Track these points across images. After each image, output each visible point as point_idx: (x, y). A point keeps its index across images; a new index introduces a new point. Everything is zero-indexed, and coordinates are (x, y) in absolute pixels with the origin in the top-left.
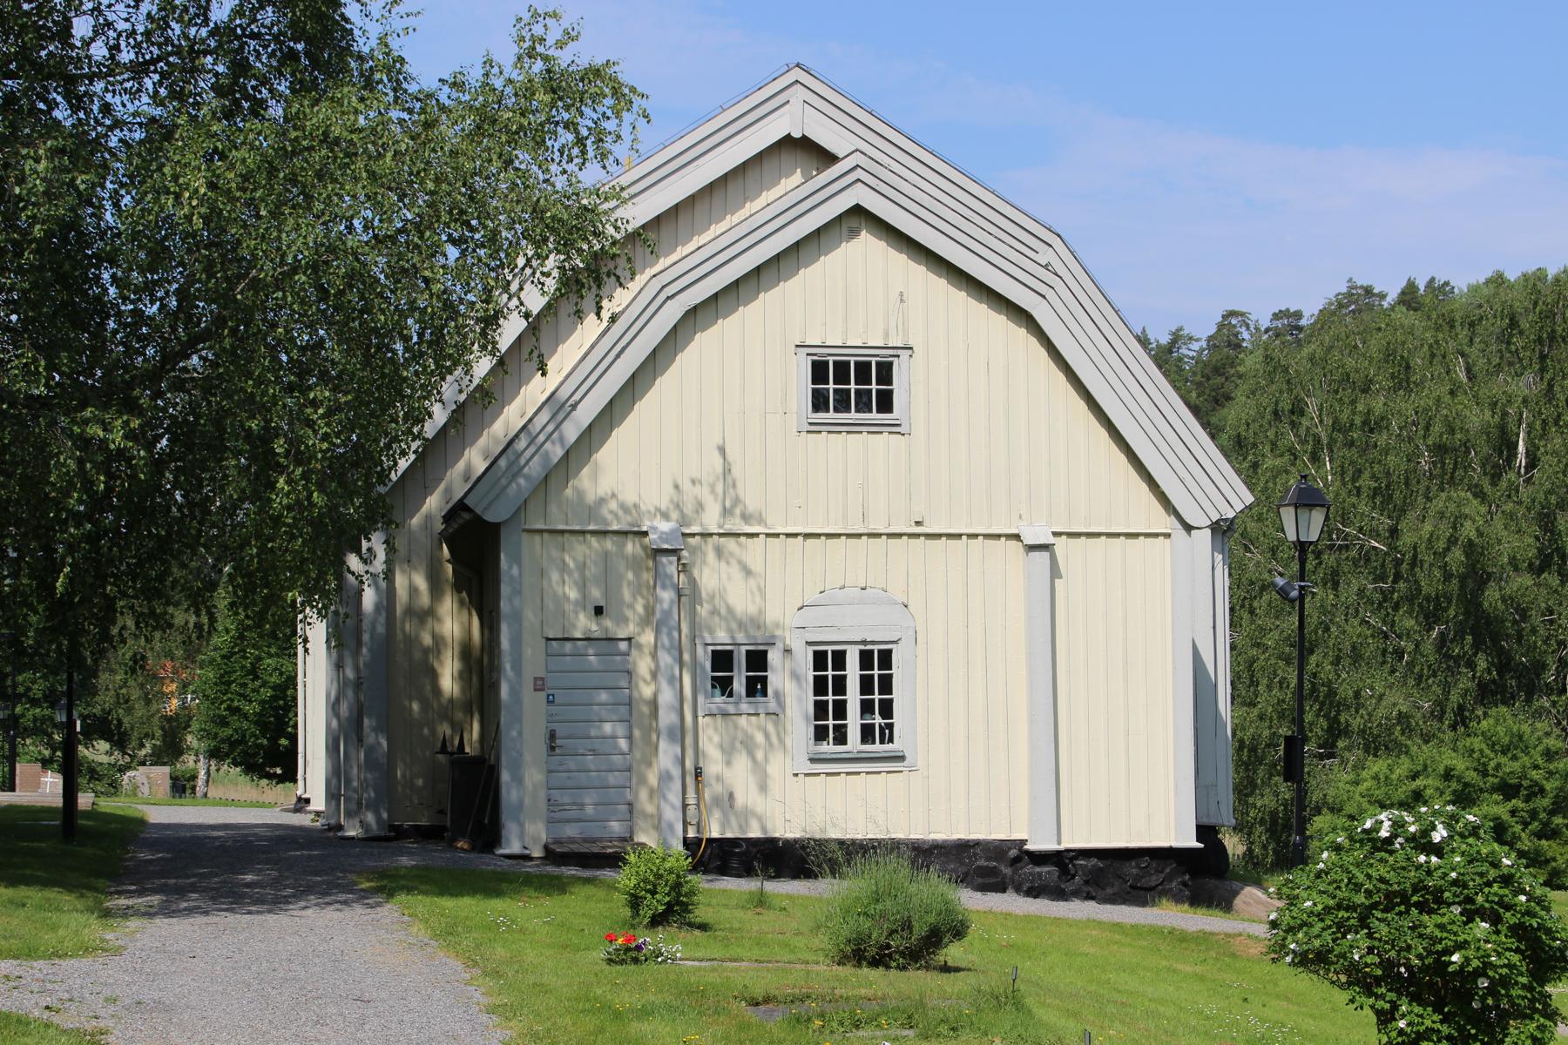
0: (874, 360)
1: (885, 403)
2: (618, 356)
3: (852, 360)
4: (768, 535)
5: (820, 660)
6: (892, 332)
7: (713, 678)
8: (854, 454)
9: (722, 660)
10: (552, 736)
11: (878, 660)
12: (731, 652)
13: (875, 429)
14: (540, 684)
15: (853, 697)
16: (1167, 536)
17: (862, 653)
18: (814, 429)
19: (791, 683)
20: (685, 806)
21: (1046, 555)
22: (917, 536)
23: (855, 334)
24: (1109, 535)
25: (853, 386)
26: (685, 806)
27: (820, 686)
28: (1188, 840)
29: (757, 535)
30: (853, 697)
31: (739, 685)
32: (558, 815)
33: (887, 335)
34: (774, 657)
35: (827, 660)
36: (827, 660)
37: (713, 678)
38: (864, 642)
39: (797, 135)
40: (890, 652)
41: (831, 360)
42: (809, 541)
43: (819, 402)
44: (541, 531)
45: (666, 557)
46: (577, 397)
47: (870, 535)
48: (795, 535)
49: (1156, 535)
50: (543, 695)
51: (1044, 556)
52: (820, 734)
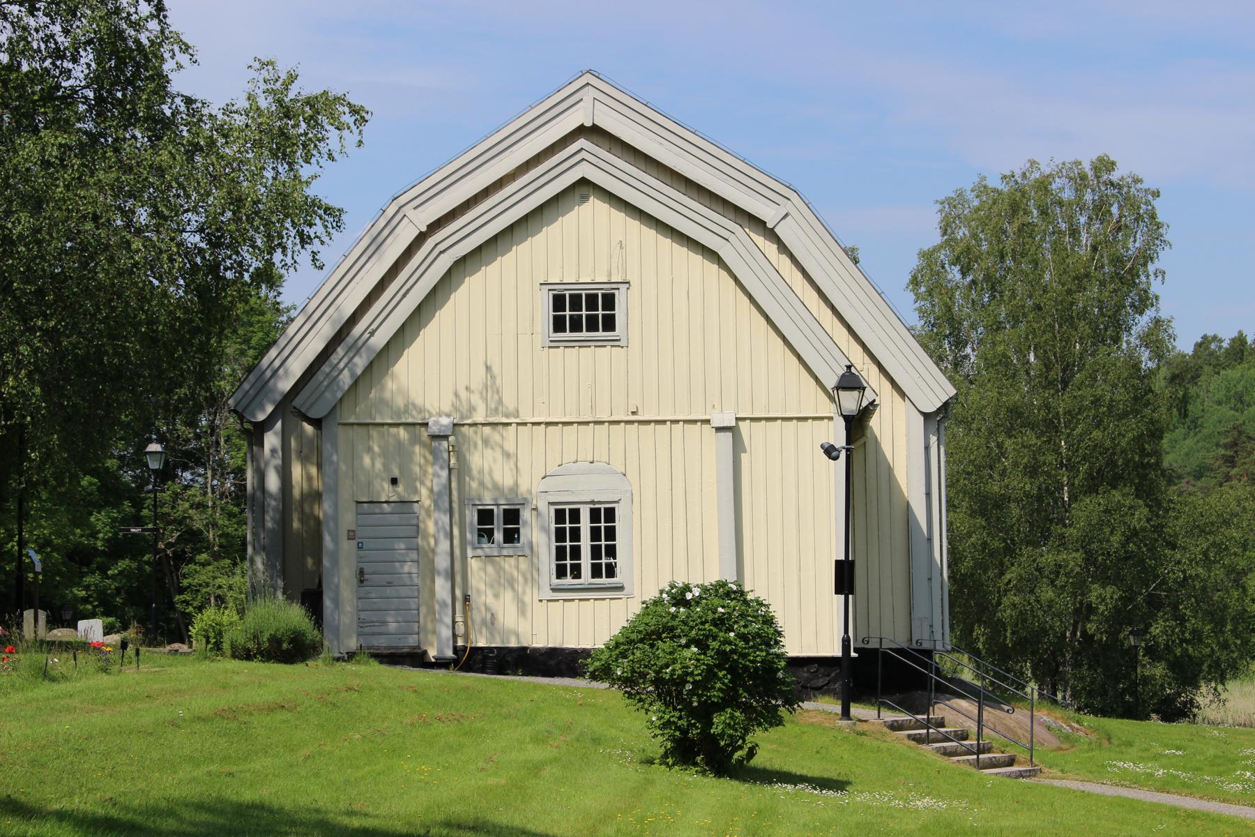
0: (600, 293)
1: (610, 324)
2: (404, 296)
3: (584, 293)
4: (518, 424)
5: (560, 516)
6: (614, 271)
7: (479, 530)
8: (586, 360)
9: (485, 516)
10: (361, 572)
11: (604, 516)
12: (518, 511)
13: (601, 343)
14: (351, 535)
15: (585, 543)
16: (831, 418)
17: (592, 510)
18: (554, 344)
19: (538, 533)
20: (454, 622)
21: (730, 434)
22: (632, 422)
23: (585, 273)
24: (784, 419)
25: (584, 313)
26: (454, 622)
27: (560, 535)
28: (838, 653)
29: (510, 424)
30: (585, 543)
31: (499, 536)
32: (367, 630)
33: (610, 275)
34: (525, 515)
35: (566, 517)
36: (566, 517)
37: (479, 530)
38: (593, 502)
39: (588, 124)
40: (613, 510)
41: (567, 293)
42: (550, 428)
43: (559, 325)
44: (352, 424)
45: (448, 442)
46: (374, 326)
47: (596, 423)
48: (539, 424)
49: (822, 418)
50: (354, 543)
51: (728, 436)
52: (561, 572)
